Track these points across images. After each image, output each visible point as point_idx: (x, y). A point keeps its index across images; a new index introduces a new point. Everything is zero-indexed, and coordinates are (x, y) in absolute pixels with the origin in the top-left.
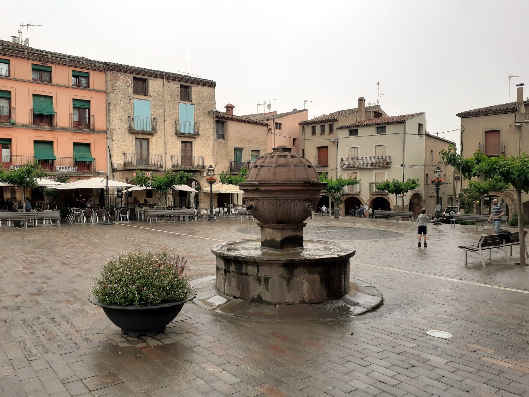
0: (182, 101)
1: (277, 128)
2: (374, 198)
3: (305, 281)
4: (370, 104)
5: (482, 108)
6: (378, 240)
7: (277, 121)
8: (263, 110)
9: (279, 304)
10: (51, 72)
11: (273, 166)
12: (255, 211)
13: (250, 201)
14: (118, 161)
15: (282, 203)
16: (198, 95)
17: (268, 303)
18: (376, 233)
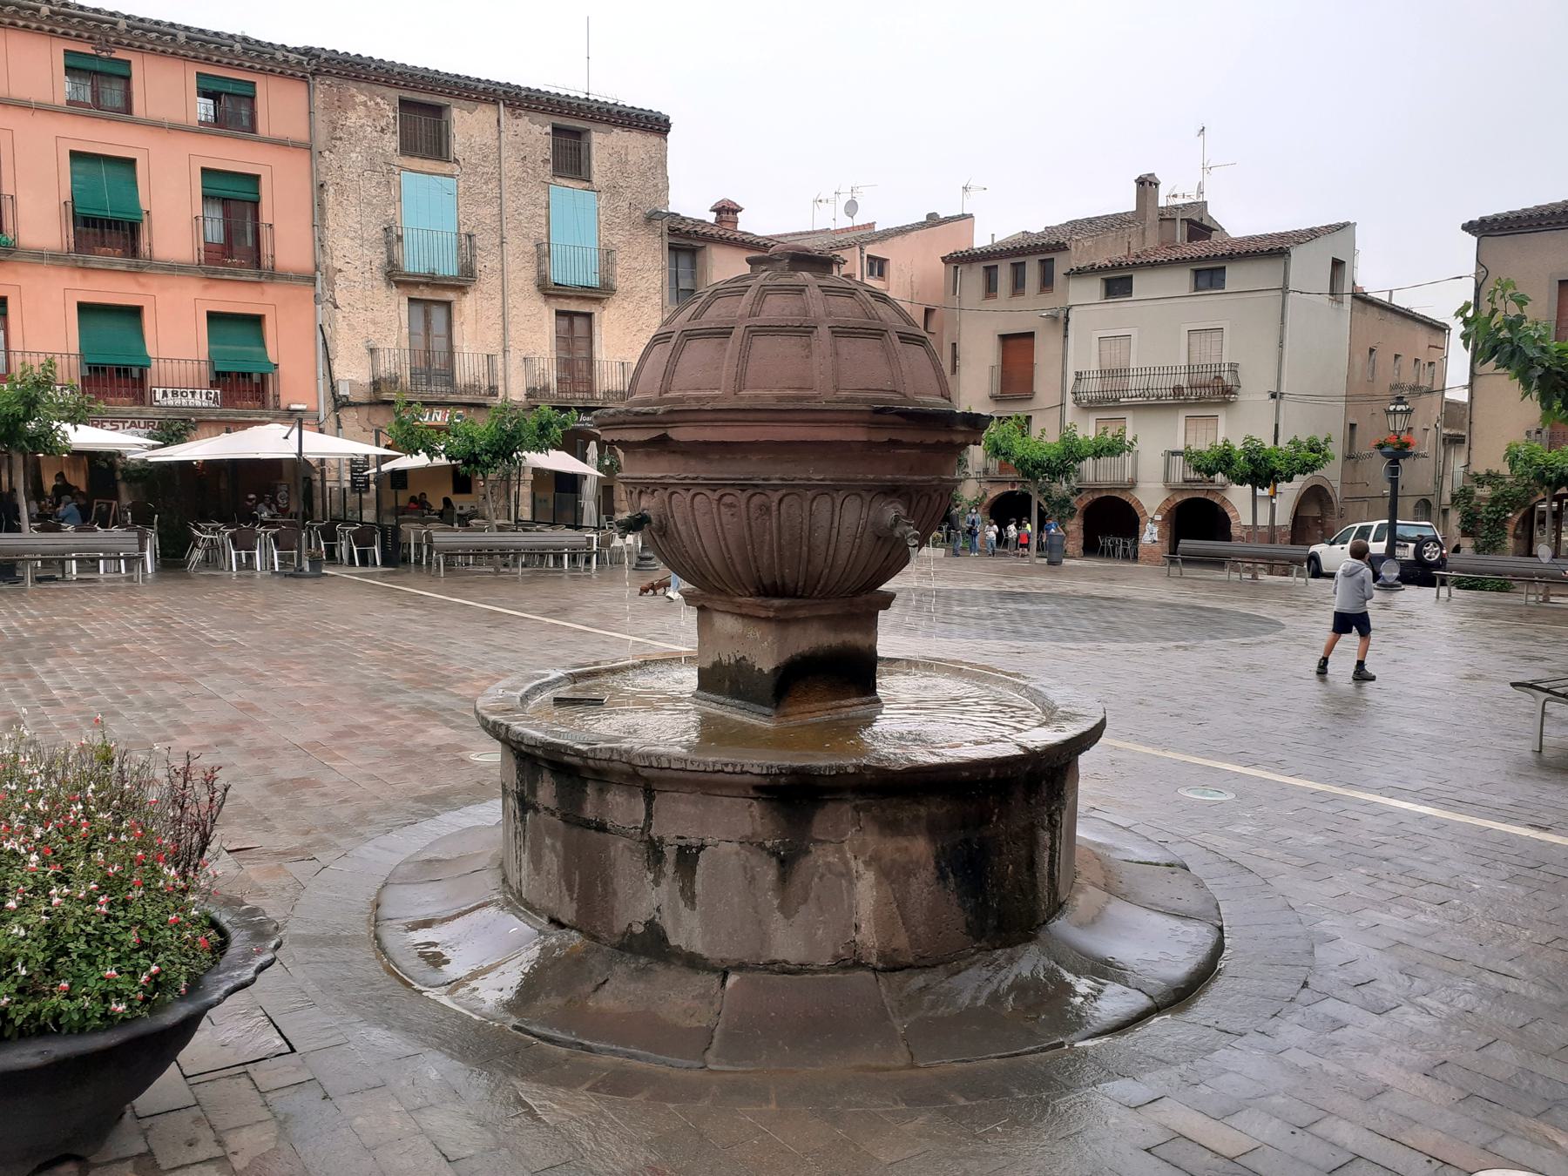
0: (558, 180)
1: (871, 273)
2: (1179, 500)
3: (861, 867)
4: (1175, 196)
5: (1552, 204)
6: (1193, 642)
7: (870, 250)
8: (831, 219)
9: (740, 967)
10: (127, 78)
11: (738, 332)
12: (660, 536)
13: (641, 492)
14: (353, 374)
15: (774, 505)
16: (612, 159)
17: (694, 962)
18: (1184, 618)
